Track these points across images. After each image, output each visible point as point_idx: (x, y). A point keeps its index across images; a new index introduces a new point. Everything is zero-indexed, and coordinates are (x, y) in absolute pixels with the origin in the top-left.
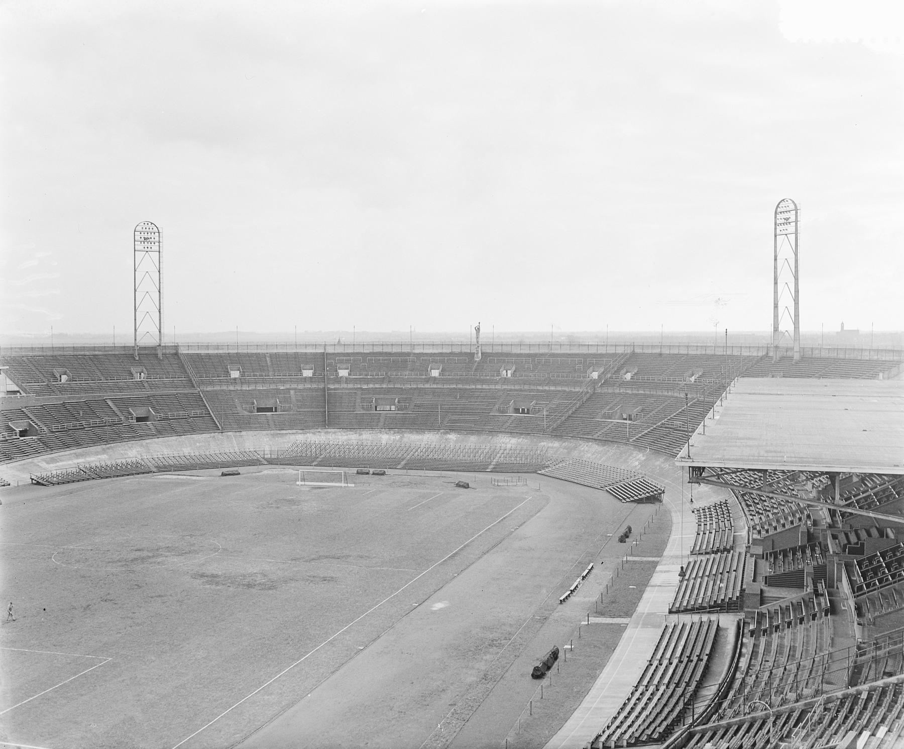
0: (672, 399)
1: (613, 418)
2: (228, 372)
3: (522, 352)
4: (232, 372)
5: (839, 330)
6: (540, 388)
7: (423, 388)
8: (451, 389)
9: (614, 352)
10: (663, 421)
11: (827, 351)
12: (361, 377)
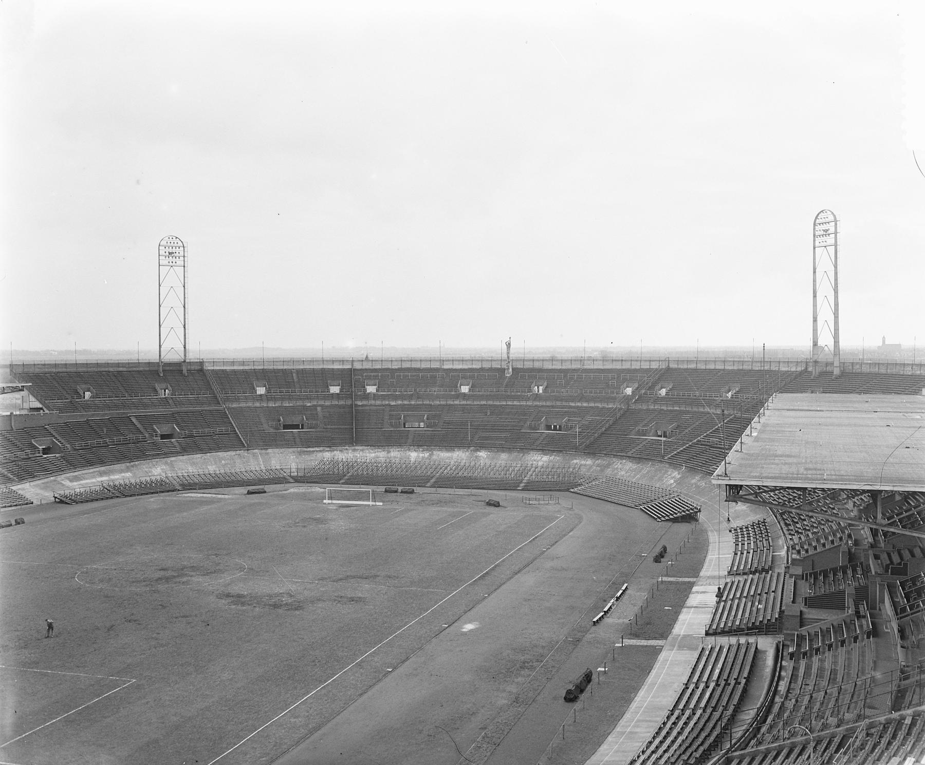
3: (554, 367)
4: (257, 388)
5: (881, 344)
7: (452, 405)
9: (648, 367)
12: (389, 393)
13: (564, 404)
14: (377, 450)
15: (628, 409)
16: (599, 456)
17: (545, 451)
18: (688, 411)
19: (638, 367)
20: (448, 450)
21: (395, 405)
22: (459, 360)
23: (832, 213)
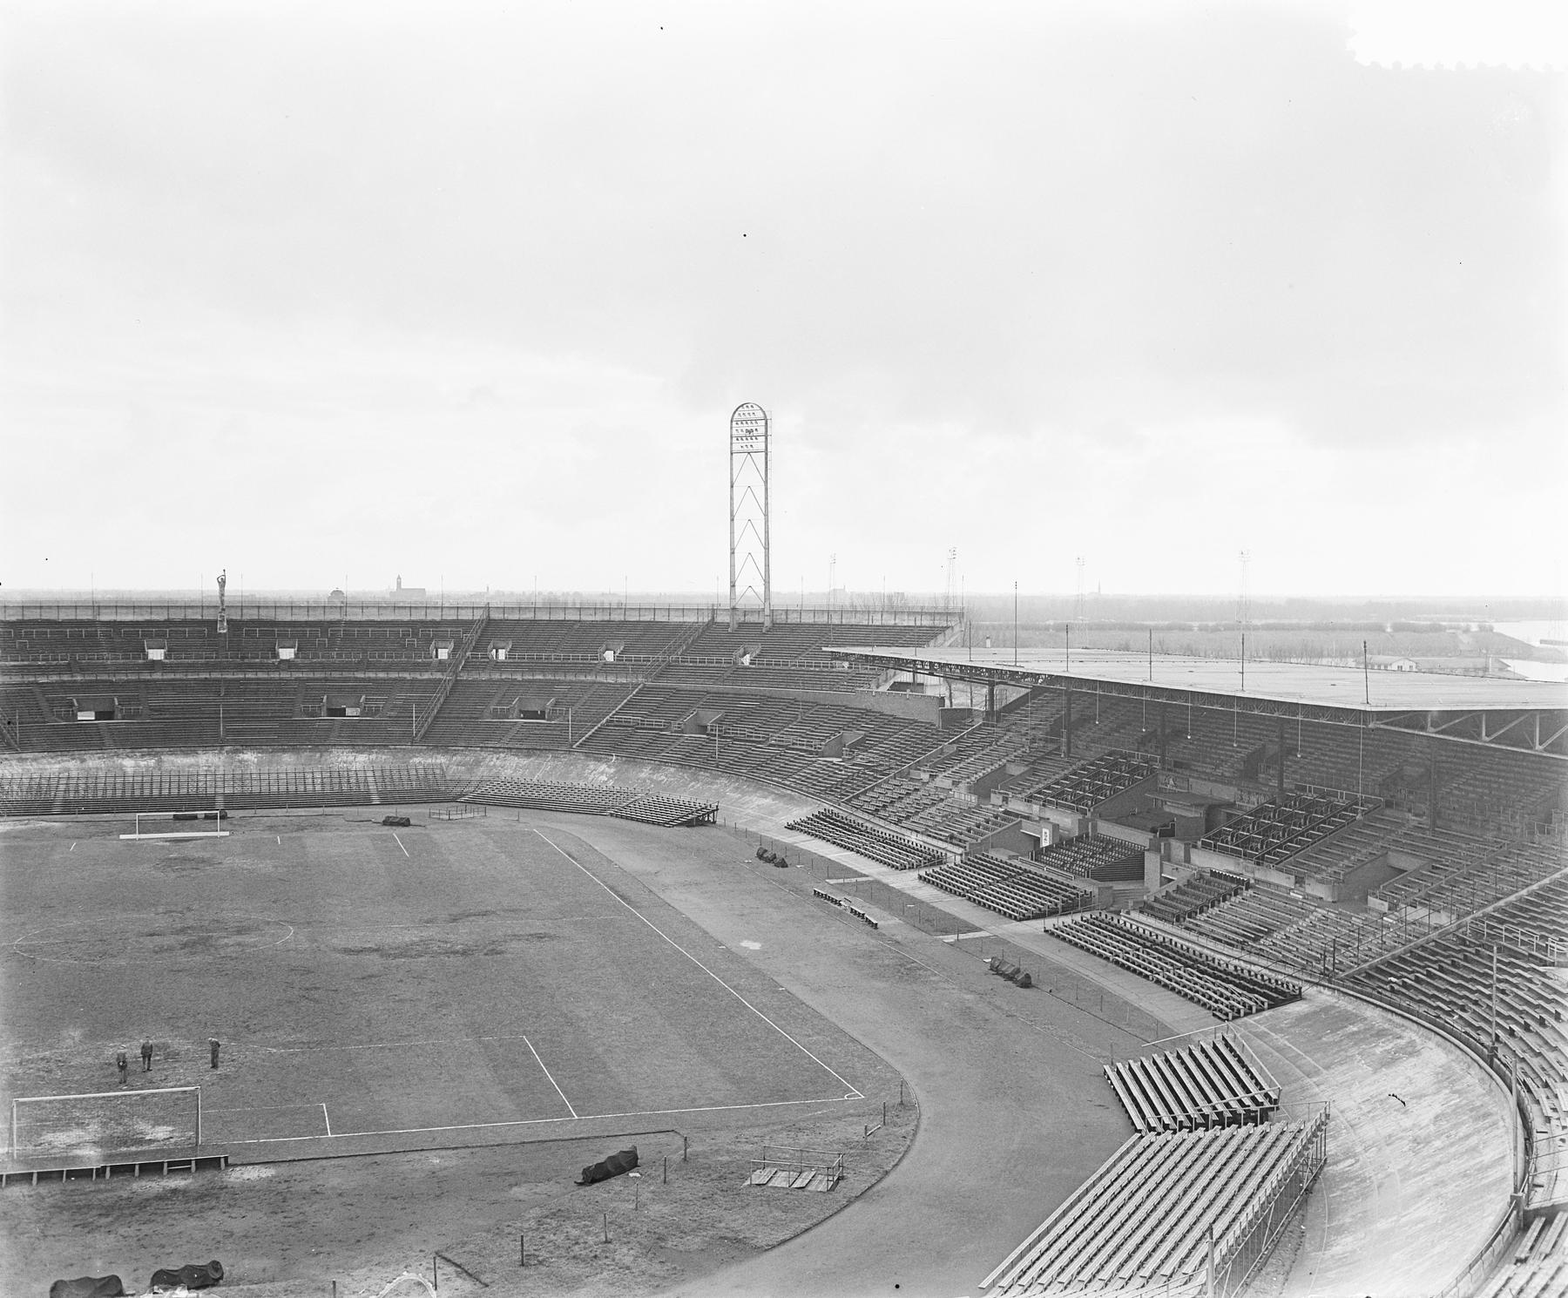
0: (596, 686)
1: (511, 716)
2: (144, 650)
3: (295, 618)
4: (150, 651)
5: (394, 588)
6: (360, 675)
7: (148, 681)
8: (201, 680)
9: (455, 618)
10: (608, 717)
11: (812, 615)
12: (26, 663)
13: (346, 674)
14: (60, 759)
15: (457, 680)
16: (455, 750)
17: (357, 747)
18: (559, 680)
19: (438, 619)
20: (186, 754)
21: (47, 683)
22: (127, 607)
23: (761, 409)
